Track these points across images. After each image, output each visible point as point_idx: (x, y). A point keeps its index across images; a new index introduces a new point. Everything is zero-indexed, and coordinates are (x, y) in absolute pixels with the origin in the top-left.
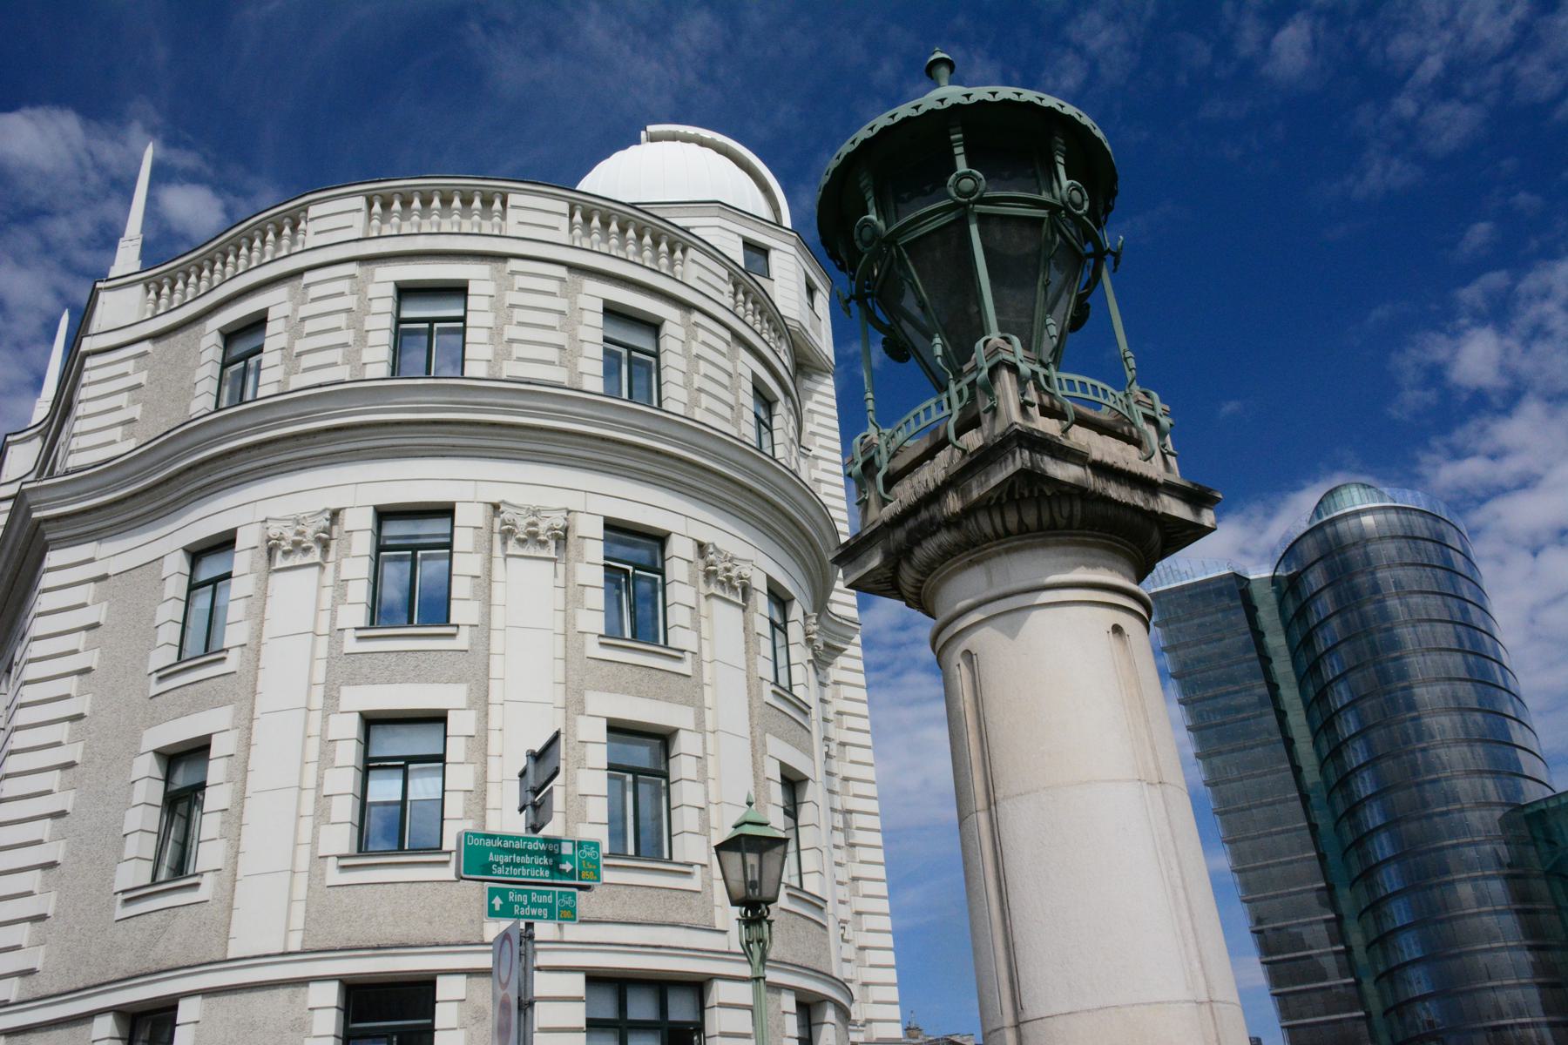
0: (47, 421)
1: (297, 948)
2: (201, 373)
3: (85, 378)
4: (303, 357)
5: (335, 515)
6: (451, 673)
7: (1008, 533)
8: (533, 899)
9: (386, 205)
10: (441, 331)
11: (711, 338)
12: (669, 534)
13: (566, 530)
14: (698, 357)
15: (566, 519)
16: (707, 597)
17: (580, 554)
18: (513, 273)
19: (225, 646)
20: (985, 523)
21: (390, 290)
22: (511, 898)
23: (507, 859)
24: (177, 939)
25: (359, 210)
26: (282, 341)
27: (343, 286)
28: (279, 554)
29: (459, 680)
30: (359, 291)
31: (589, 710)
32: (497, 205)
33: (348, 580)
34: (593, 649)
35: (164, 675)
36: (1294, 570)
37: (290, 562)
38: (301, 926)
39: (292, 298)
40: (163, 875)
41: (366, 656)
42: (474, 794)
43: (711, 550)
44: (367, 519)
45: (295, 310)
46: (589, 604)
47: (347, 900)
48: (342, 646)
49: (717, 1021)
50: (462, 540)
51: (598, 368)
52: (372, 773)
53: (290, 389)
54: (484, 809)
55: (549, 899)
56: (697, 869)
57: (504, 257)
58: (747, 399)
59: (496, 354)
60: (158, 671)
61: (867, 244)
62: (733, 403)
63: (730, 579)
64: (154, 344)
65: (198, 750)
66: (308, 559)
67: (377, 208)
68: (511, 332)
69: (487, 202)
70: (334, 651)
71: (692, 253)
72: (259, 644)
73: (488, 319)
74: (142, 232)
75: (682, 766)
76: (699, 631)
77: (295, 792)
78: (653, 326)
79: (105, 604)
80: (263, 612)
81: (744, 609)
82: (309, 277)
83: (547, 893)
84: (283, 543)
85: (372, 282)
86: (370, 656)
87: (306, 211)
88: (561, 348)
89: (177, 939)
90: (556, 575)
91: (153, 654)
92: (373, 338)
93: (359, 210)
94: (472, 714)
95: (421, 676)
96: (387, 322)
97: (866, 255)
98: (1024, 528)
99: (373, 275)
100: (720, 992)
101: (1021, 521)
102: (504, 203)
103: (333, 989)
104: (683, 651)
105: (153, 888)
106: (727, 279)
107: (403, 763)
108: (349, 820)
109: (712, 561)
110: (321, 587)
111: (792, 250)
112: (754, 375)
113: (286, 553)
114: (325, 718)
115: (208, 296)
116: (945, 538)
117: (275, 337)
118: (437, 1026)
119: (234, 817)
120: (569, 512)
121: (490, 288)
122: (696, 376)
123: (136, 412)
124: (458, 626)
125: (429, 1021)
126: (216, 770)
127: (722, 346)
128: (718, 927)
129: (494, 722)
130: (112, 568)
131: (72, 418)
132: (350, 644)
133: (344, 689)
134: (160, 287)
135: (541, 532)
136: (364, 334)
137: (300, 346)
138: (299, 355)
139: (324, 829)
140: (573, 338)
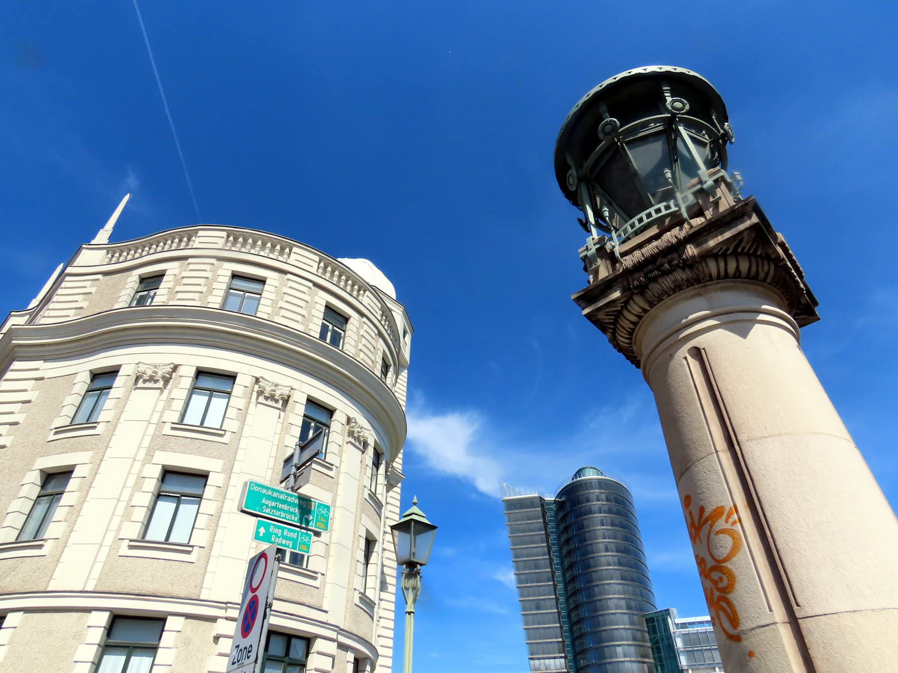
0: (35, 309)
1: (91, 589)
2: (124, 292)
3: (63, 285)
4: (179, 293)
5: (175, 368)
6: (216, 453)
7: (727, 276)
8: (285, 533)
9: (236, 240)
10: (249, 297)
11: (368, 329)
12: (336, 410)
13: (289, 397)
14: (363, 336)
15: (290, 391)
16: (347, 443)
17: (293, 409)
18: (288, 280)
19: (98, 420)
20: (712, 267)
21: (229, 274)
22: (271, 530)
23: (273, 504)
24: (20, 576)
25: (222, 237)
26: (170, 285)
27: (207, 267)
28: (141, 380)
29: (220, 458)
32: (287, 250)
33: (174, 399)
35: (59, 431)
36: (564, 499)
37: (148, 385)
39: (180, 267)
40: (24, 537)
41: (174, 437)
42: (214, 517)
43: (353, 421)
44: (192, 372)
45: (180, 273)
47: (128, 565)
48: (162, 431)
49: (314, 661)
51: (319, 329)
52: (160, 497)
53: (169, 304)
54: (217, 526)
55: (295, 536)
56: (319, 576)
57: (285, 272)
59: (273, 312)
60: (56, 428)
61: (607, 134)
63: (359, 436)
64: (103, 276)
65: (65, 473)
66: (156, 385)
67: (231, 238)
69: (283, 249)
70: (157, 432)
71: (367, 293)
72: (117, 423)
74: (113, 228)
76: (341, 457)
77: (132, 459)
78: (346, 319)
79: (38, 392)
80: (124, 407)
81: (363, 452)
82: (190, 260)
83: (294, 531)
84: (145, 375)
85: (221, 268)
86: (176, 437)
87: (197, 233)
88: (303, 316)
89: (20, 576)
90: (279, 418)
91: (56, 419)
92: (215, 292)
93: (222, 237)
94: (222, 476)
95: (201, 453)
96: (224, 286)
97: (604, 142)
98: (738, 273)
99: (222, 266)
100: (319, 645)
101: (738, 268)
102: (290, 251)
104: (332, 465)
105: (17, 544)
106: (380, 308)
107: (179, 495)
108: (142, 521)
109: (353, 426)
110: (158, 400)
111: (401, 313)
112: (384, 350)
113: (145, 381)
114: (143, 465)
115: (138, 259)
116: (680, 275)
117: (166, 283)
118: (160, 646)
119: (75, 510)
120: (292, 389)
121: (277, 283)
122: (360, 344)
123: (85, 304)
124: (225, 431)
126: (73, 484)
127: (373, 335)
128: (324, 608)
130: (47, 375)
131: (51, 302)
132: (167, 430)
133: (157, 452)
134: (115, 252)
135: (276, 395)
136: (212, 290)
137: (178, 288)
138: (177, 292)
140: (310, 313)
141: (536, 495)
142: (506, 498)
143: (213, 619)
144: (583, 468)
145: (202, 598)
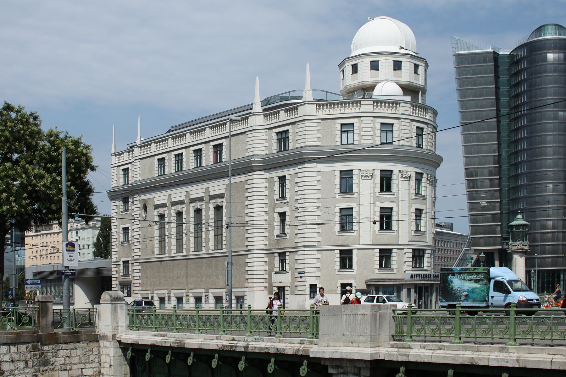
21: (340, 125)
27: (370, 122)
30: (374, 124)
38: (158, 235)
39: (359, 122)
50: (355, 177)
68: (362, 134)
73: (358, 131)
102: (360, 104)
103: (378, 250)
113: (365, 177)
121: (398, 125)
125: (342, 256)
129: (400, 209)
141: (490, 50)
142: (457, 52)
143: (403, 249)
144: (545, 25)
145: (399, 244)
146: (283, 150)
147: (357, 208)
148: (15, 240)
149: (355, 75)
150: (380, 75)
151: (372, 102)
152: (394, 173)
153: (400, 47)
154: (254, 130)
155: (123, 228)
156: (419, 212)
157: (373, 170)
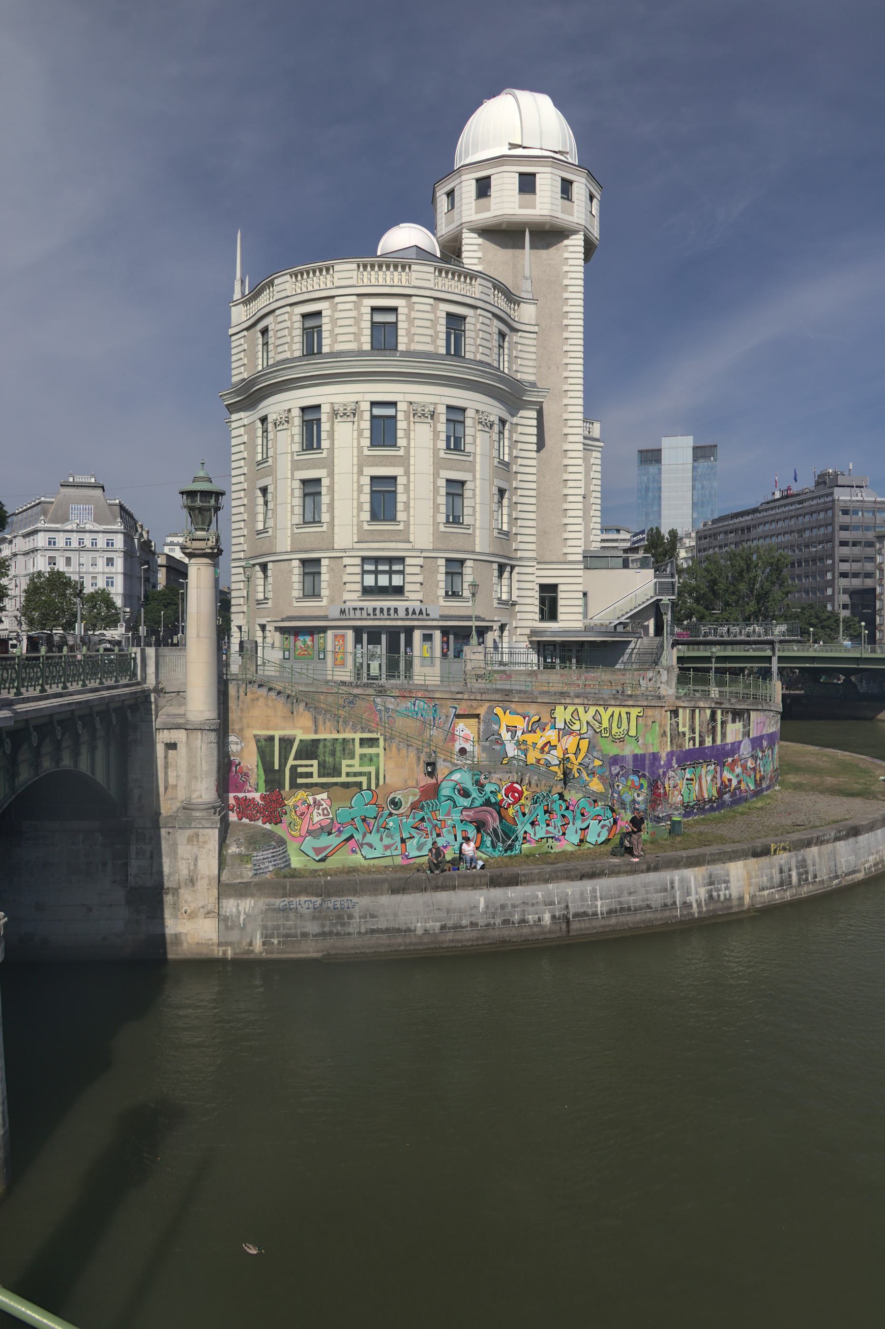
21: (369, 310)
31: (441, 476)
34: (442, 454)
46: (441, 494)
58: (496, 337)
62: (490, 347)
68: (413, 330)
75: (467, 494)
96: (368, 324)
126: (325, 320)
139: (362, 478)
146: (316, 352)
147: (405, 478)
148: (847, 496)
149: (483, 201)
150: (493, 207)
151: (288, 276)
152: (400, 406)
153: (510, 144)
154: (273, 311)
155: (449, 481)
156: (455, 489)
157: (357, 403)
